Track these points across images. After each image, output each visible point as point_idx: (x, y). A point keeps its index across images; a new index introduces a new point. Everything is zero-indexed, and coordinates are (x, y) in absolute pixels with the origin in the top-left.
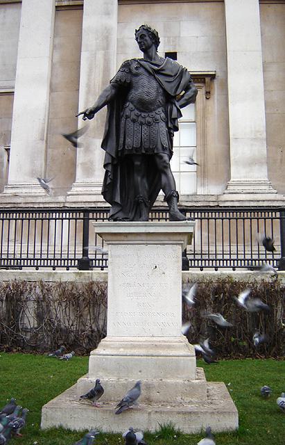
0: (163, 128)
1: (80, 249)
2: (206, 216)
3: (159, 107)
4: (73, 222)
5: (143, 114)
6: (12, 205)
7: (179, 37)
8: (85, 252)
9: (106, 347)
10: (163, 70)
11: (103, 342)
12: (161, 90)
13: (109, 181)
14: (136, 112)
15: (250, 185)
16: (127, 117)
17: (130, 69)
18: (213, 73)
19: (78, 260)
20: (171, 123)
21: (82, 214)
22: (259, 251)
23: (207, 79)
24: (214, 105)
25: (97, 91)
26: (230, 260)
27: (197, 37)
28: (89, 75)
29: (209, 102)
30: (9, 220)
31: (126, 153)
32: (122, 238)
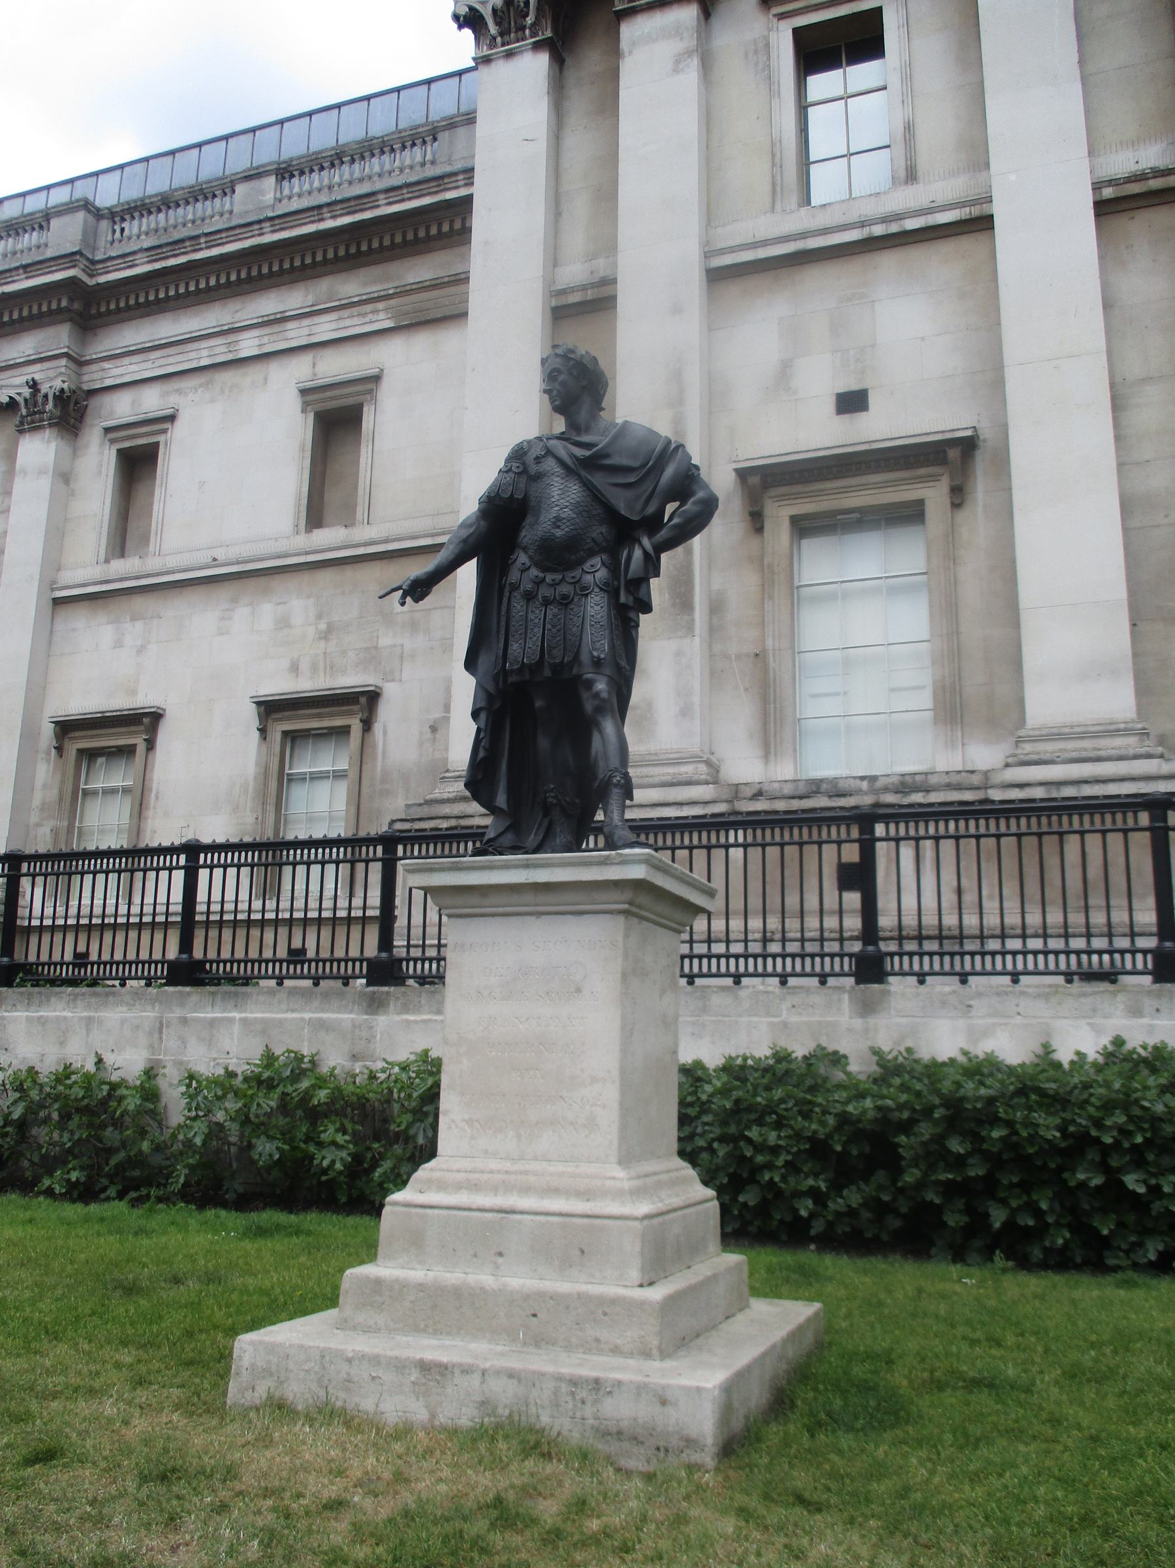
0: (595, 607)
3: (592, 554)
4: (755, 853)
5: (549, 578)
6: (453, 823)
9: (430, 1184)
10: (607, 456)
11: (425, 1171)
12: (598, 510)
13: (481, 754)
14: (534, 572)
15: (1082, 736)
16: (515, 587)
17: (524, 464)
18: (969, 433)
20: (628, 591)
21: (380, 849)
23: (953, 454)
24: (977, 522)
27: (923, 339)
29: (962, 515)
31: (512, 679)
32: (475, 899)
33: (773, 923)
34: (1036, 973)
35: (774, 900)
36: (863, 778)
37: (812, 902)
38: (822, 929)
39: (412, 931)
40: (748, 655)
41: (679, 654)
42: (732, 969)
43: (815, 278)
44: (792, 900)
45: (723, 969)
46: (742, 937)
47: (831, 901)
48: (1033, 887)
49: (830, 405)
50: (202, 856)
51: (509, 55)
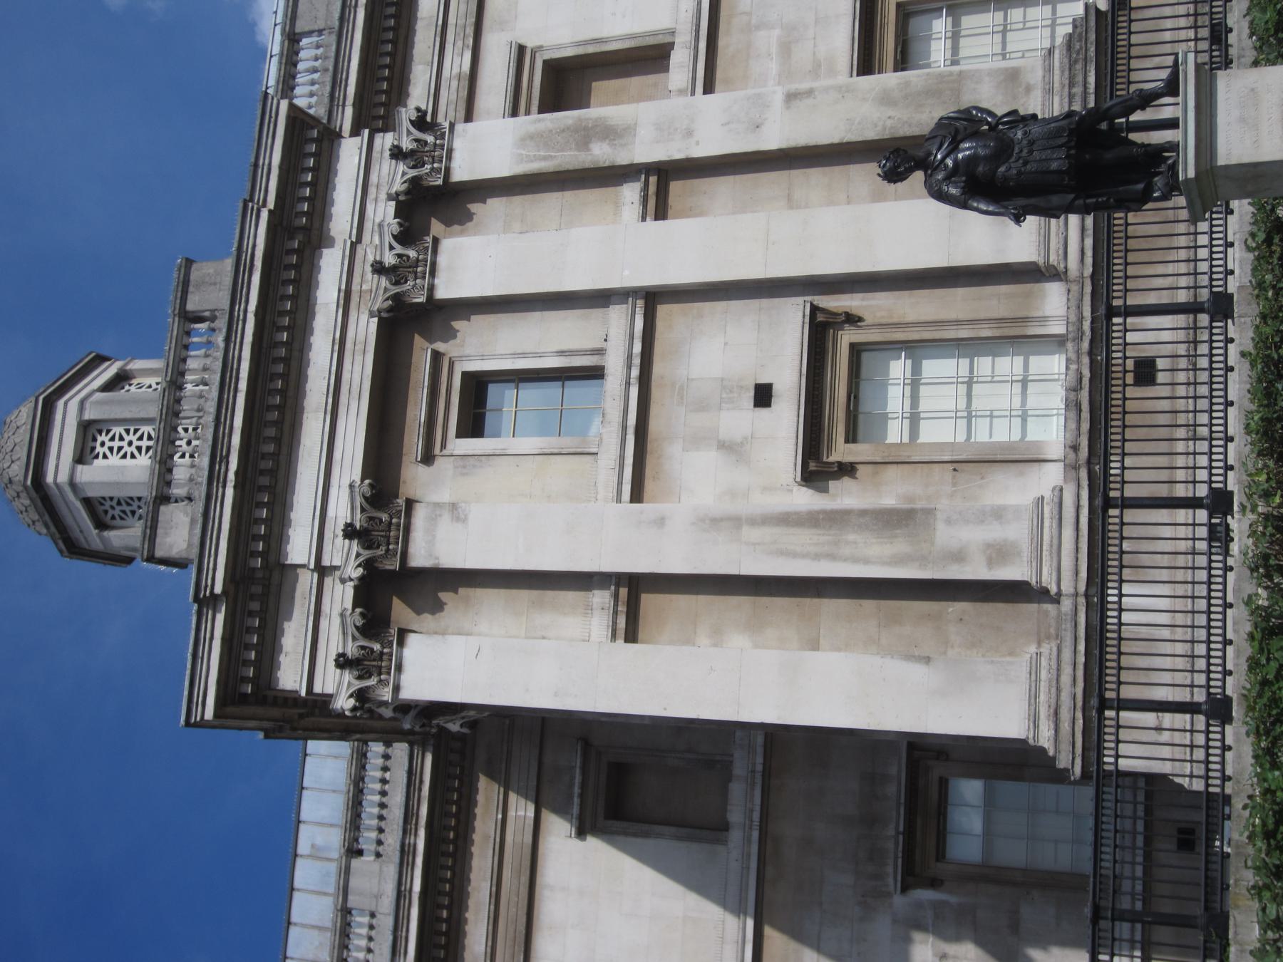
1: (1182, 515)
2: (1114, 672)
4: (1124, 676)
7: (722, 380)
8: (1192, 503)
19: (1212, 321)
21: (1115, 320)
22: (1187, 454)
25: (826, 538)
26: (1212, 273)
27: (726, 344)
28: (794, 555)
29: (869, 319)
30: (1120, 668)
33: (1181, 433)
34: (1226, 390)
35: (1163, 433)
36: (1067, 368)
37: (1165, 405)
38: (1187, 370)
39: (1177, 757)
40: (954, 477)
41: (949, 522)
42: (1221, 407)
43: (656, 425)
44: (1163, 419)
45: (1220, 654)
46: (1191, 528)
47: (1165, 391)
48: (1163, 242)
49: (763, 412)
50: (1106, 767)
51: (399, 668)
